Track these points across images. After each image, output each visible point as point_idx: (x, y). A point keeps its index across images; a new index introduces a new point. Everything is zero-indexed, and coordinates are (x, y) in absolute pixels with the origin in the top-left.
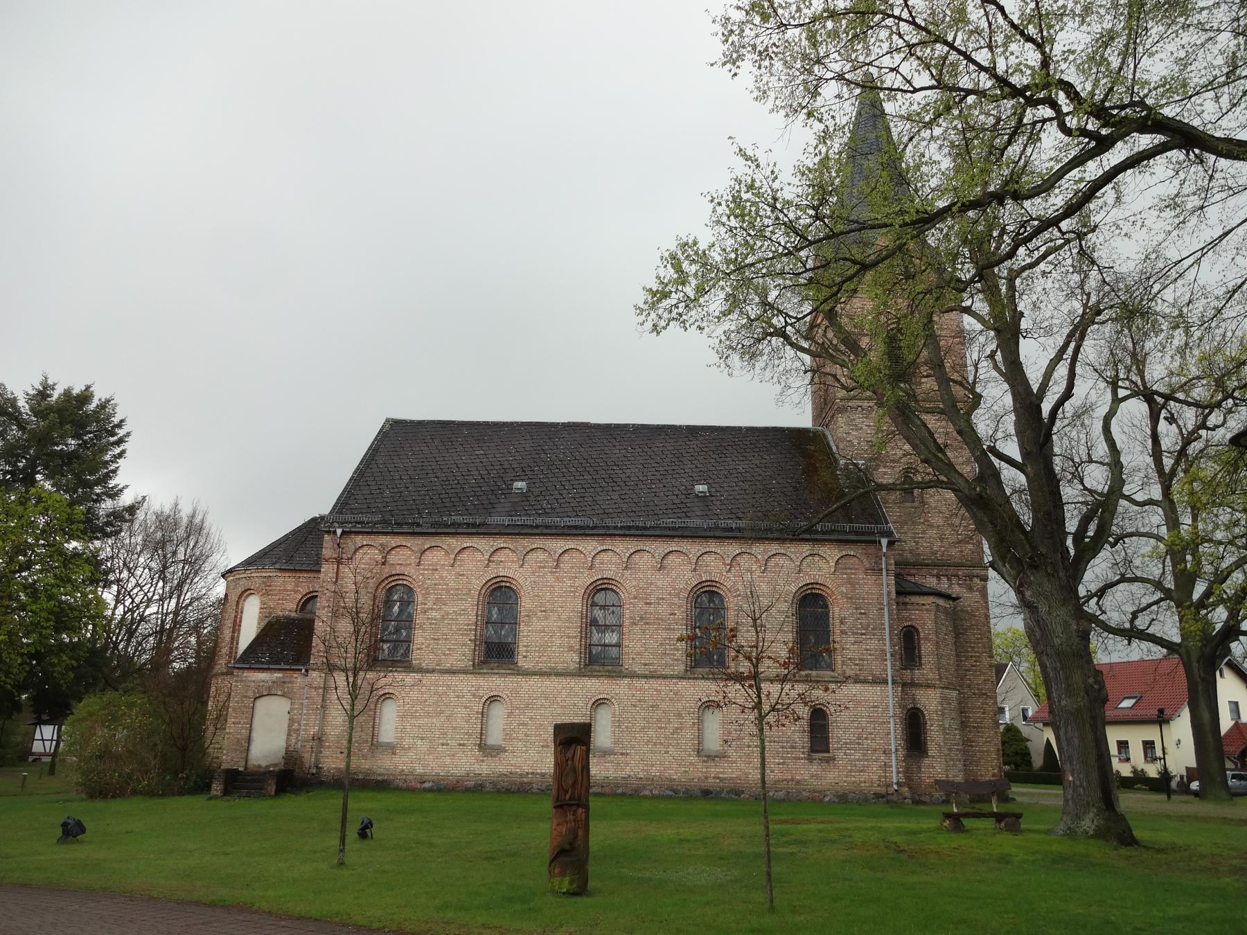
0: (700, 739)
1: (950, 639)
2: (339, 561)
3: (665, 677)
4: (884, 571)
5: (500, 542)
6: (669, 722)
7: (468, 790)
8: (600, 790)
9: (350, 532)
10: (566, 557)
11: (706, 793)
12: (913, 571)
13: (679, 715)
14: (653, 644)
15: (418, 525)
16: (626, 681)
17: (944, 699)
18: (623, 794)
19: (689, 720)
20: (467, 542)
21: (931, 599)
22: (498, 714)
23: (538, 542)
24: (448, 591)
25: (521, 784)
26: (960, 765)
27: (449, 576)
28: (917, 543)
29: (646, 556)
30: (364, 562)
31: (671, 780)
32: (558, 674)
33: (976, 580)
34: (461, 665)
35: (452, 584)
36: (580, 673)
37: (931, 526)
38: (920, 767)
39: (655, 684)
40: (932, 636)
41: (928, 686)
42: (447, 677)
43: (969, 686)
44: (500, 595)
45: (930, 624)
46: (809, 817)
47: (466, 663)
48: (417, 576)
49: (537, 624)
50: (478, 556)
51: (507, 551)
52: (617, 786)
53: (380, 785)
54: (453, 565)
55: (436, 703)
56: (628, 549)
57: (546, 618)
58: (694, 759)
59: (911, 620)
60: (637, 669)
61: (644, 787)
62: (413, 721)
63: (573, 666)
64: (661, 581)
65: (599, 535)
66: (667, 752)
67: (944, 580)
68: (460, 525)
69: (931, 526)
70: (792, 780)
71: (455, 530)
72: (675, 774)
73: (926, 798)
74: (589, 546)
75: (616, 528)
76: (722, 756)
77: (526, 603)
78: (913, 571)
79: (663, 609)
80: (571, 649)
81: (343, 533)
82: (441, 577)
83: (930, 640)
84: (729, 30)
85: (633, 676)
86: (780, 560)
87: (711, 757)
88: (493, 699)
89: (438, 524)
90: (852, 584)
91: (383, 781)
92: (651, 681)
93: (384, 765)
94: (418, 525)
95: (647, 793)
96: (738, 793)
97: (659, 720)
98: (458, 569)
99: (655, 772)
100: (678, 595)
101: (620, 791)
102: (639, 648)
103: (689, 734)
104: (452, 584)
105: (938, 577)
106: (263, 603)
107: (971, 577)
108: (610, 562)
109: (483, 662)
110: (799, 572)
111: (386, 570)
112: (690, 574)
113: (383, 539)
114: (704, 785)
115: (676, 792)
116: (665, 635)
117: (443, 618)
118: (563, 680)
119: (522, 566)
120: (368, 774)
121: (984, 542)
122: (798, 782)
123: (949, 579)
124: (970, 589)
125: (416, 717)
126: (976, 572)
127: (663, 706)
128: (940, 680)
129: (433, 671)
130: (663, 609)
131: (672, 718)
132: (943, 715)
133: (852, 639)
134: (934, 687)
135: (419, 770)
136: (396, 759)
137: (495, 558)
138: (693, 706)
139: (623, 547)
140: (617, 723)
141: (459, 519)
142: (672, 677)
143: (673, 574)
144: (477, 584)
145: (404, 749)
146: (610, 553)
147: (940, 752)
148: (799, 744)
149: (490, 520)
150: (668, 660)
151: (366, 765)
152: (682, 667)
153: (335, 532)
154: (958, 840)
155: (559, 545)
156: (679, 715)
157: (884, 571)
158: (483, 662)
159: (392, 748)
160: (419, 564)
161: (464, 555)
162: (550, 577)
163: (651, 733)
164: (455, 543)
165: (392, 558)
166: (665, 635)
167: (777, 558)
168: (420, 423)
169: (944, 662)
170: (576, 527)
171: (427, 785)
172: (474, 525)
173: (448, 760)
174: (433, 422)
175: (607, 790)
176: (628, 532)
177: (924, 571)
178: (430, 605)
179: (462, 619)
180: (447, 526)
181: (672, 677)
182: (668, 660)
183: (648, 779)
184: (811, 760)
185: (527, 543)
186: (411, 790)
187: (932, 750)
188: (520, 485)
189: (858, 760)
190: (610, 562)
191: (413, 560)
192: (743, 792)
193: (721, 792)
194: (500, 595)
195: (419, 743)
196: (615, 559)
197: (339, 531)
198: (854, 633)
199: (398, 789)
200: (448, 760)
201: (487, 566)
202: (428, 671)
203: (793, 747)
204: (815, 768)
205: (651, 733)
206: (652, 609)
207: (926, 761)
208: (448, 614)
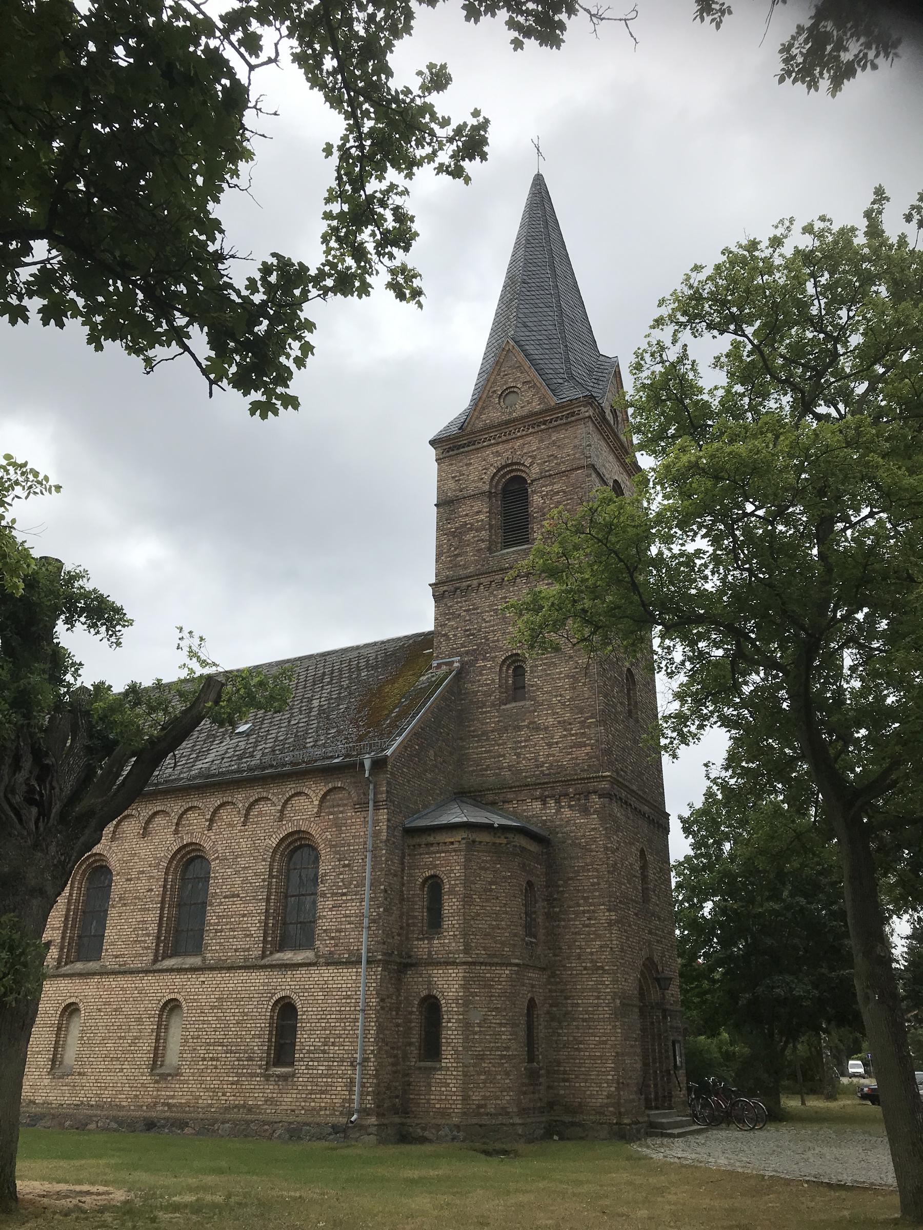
3: (132, 972)
4: (371, 804)
6: (129, 1030)
11: (150, 1125)
12: (510, 796)
13: (139, 1020)
19: (149, 1026)
28: (518, 755)
37: (537, 729)
38: (429, 1085)
39: (122, 981)
41: (447, 963)
43: (579, 957)
45: (458, 871)
46: (507, 1147)
58: (146, 1079)
59: (436, 866)
69: (537, 729)
70: (244, 1106)
76: (177, 1073)
78: (510, 796)
84: (906, 236)
86: (265, 807)
88: (171, 1007)
90: (338, 825)
92: (119, 978)
103: (147, 1045)
105: (544, 801)
112: (171, 838)
121: (248, 726)
122: (250, 1110)
123: (558, 802)
124: (585, 811)
128: (467, 950)
133: (330, 903)
134: (454, 963)
138: (154, 1007)
147: (457, 1060)
150: (138, 949)
156: (139, 1020)
157: (371, 804)
182: (138, 949)
189: (322, 1076)
192: (187, 1124)
198: (333, 894)
203: (250, 1059)
204: (270, 1089)
207: (439, 1076)
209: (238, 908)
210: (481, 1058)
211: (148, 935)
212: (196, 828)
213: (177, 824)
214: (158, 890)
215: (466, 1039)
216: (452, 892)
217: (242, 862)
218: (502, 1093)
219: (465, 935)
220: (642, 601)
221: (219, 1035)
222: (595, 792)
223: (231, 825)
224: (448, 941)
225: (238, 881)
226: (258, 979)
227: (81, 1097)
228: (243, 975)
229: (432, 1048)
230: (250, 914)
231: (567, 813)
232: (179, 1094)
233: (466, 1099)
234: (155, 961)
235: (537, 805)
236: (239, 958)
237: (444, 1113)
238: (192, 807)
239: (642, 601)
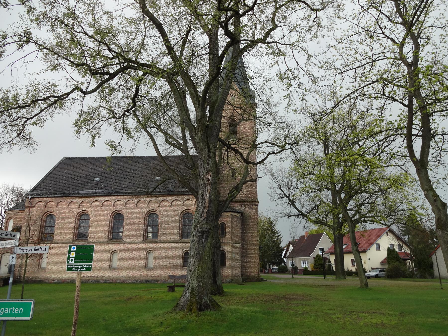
0: (146, 263)
1: (239, 227)
2: (31, 207)
3: (136, 243)
5: (84, 199)
6: (136, 258)
7: (68, 283)
8: (111, 281)
9: (34, 198)
10: (105, 203)
11: (147, 281)
12: (233, 204)
13: (140, 255)
14: (132, 232)
15: (57, 194)
16: (123, 244)
17: (233, 247)
18: (119, 283)
19: (143, 257)
20: (73, 199)
21: (230, 213)
22: (116, 257)
23: (96, 198)
24: (66, 216)
25: (86, 280)
26: (240, 270)
27: (66, 211)
29: (132, 202)
30: (38, 208)
31: (136, 277)
32: (100, 243)
33: (254, 206)
34: (69, 241)
35: (67, 214)
36: (108, 242)
39: (132, 245)
40: (230, 226)
41: (227, 243)
42: (64, 245)
43: (250, 242)
44: (151, 218)
45: (229, 222)
47: (177, 239)
48: (55, 212)
49: (94, 226)
50: (76, 204)
51: (86, 202)
52: (117, 280)
53: (40, 282)
54: (68, 207)
55: (60, 254)
56: (183, 198)
57: (98, 224)
58: (144, 270)
60: (127, 240)
61: (126, 280)
62: (52, 260)
63: (106, 240)
64: (137, 210)
65: (116, 195)
66: (135, 268)
67: (243, 206)
68: (70, 194)
71: (69, 195)
72: (137, 275)
73: (224, 281)
74: (113, 199)
75: (122, 193)
76: (153, 269)
77: (92, 219)
78: (233, 204)
79: (137, 220)
80: (105, 234)
81: (31, 198)
82: (64, 212)
83: (229, 227)
85: (125, 243)
86: (177, 202)
87: (150, 269)
89: (64, 194)
91: (41, 280)
93: (42, 275)
94: (57, 194)
95: (127, 282)
96: (157, 281)
97: (133, 257)
98: (69, 209)
99: (130, 275)
100: (142, 215)
101: (118, 281)
102: (128, 233)
103: (143, 262)
104: (67, 214)
105: (241, 205)
106: (14, 222)
107: (253, 205)
108: (120, 204)
109: (77, 240)
110: (183, 206)
111: (46, 210)
112: (146, 208)
113: (45, 199)
114: (146, 279)
115: (137, 281)
116: (136, 228)
117: (64, 225)
118: (102, 245)
119: (90, 207)
120: (36, 278)
123: (245, 206)
124: (252, 209)
125: (53, 259)
126: (254, 203)
127: (134, 252)
128: (232, 240)
129: (59, 243)
130: (137, 220)
131: (137, 256)
132: (232, 253)
135: (53, 276)
136: (46, 273)
137: (82, 204)
139: (124, 199)
140: (119, 259)
141: (71, 192)
142: (138, 243)
143: (141, 208)
144: (75, 213)
145: (48, 269)
146: (120, 202)
148: (179, 264)
149: (81, 191)
150: (137, 237)
151: (36, 275)
152: (142, 239)
153: (28, 198)
154: (173, 294)
155: (103, 199)
156: (140, 255)
158: (77, 240)
159: (45, 269)
160: (57, 207)
161: (72, 204)
162: (100, 210)
163: (130, 262)
164: (69, 200)
165: (48, 206)
166: (136, 228)
167: (176, 201)
168: (75, 158)
169: (234, 235)
170: (109, 193)
171: (55, 281)
172: (75, 194)
173: (63, 273)
174: (79, 158)
175: (114, 281)
176: (125, 194)
177: (236, 204)
178: (60, 221)
179: (70, 225)
180: (66, 194)
181: (138, 243)
182: (137, 237)
183: (128, 277)
184: (182, 269)
185: (92, 199)
186: (50, 283)
187: (228, 264)
188: (97, 179)
190: (120, 204)
191: (55, 206)
193: (151, 281)
194: (117, 218)
195: (54, 267)
196: (121, 203)
197: (30, 197)
199: (46, 283)
200: (63, 273)
201: (79, 207)
202: (57, 243)
205: (130, 262)
206: (133, 220)
207: (225, 269)
208: (65, 224)
209: (132, 230)
210: (234, 265)
211: (140, 233)
212: (86, 207)
213: (80, 205)
214: (142, 221)
215: (232, 261)
216: (228, 227)
217: (171, 216)
218: (238, 273)
219: (232, 237)
220: (37, 100)
221: (167, 259)
222: (255, 205)
223: (166, 206)
224: (227, 238)
225: (170, 221)
226: (178, 246)
227: (122, 275)
228: (173, 245)
229: (223, 263)
230: (174, 229)
231: (247, 209)
232: (155, 274)
233: (232, 273)
234: (143, 240)
235: (240, 206)
236: (172, 240)
237: (227, 277)
238: (140, 200)
239: (37, 100)
